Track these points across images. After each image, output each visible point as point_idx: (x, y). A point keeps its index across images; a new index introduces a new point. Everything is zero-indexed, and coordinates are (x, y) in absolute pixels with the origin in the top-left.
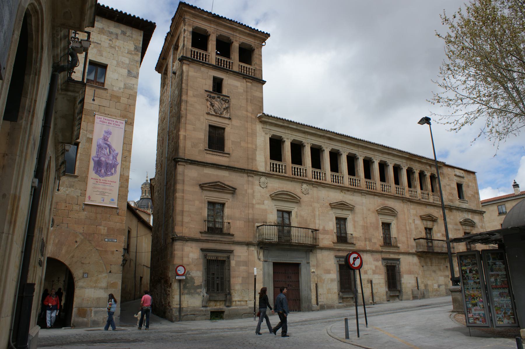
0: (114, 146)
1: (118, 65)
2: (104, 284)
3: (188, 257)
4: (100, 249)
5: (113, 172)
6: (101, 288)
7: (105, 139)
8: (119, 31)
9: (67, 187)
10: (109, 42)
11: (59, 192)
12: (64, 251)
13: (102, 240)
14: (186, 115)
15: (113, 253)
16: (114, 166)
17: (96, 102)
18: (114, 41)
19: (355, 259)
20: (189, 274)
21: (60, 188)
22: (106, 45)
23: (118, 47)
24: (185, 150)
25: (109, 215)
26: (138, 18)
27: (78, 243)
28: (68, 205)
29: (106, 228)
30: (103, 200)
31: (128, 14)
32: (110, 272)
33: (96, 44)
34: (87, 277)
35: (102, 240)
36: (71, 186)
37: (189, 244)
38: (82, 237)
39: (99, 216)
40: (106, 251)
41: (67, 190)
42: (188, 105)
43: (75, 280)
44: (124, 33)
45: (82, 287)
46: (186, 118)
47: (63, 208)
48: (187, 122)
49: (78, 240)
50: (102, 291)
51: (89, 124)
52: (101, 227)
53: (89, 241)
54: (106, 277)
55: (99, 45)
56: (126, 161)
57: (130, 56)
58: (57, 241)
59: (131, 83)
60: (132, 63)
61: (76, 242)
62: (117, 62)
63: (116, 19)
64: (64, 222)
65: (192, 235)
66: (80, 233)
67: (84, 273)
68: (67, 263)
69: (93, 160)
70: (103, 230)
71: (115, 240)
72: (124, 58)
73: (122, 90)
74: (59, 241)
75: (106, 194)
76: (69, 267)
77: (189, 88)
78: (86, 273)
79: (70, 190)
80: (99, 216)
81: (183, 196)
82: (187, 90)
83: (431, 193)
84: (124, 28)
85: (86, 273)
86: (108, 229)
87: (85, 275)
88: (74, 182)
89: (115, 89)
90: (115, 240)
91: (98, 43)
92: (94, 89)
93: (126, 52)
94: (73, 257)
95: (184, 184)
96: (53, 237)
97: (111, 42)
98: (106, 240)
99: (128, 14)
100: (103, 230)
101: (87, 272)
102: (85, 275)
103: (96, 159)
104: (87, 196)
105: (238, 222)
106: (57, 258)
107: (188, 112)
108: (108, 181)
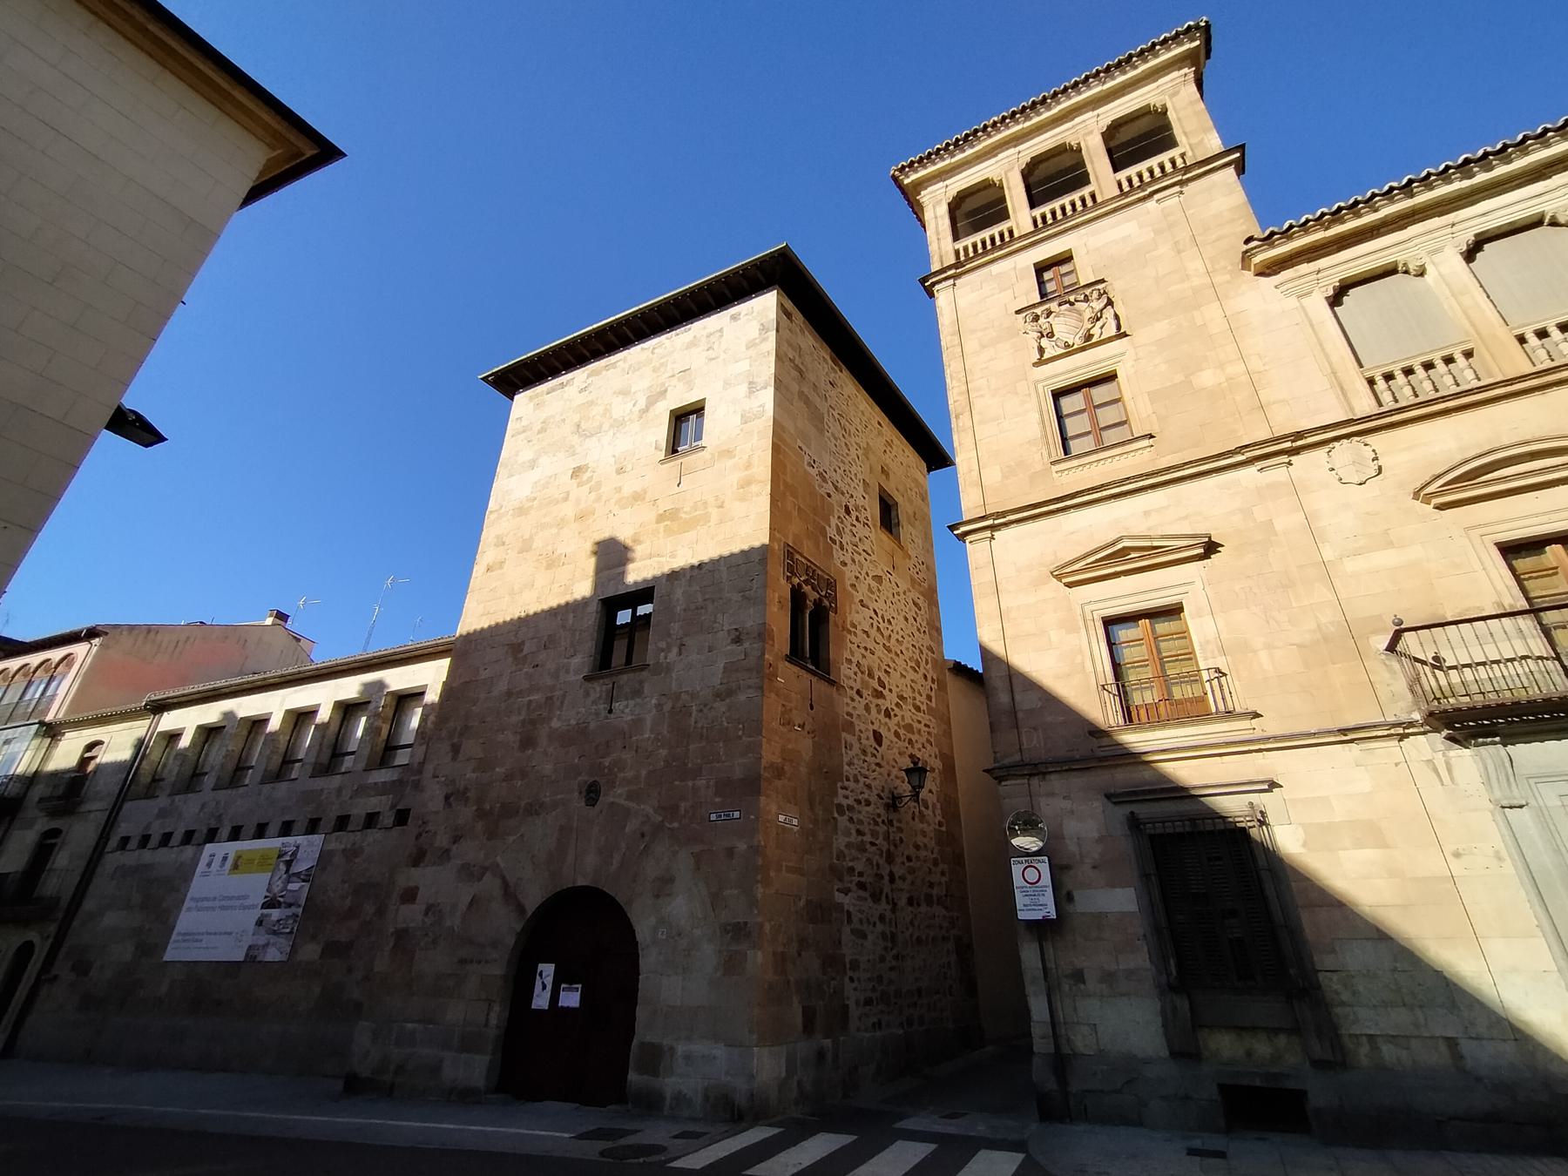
37: (1056, 782)
71: (737, 814)
90: (737, 814)
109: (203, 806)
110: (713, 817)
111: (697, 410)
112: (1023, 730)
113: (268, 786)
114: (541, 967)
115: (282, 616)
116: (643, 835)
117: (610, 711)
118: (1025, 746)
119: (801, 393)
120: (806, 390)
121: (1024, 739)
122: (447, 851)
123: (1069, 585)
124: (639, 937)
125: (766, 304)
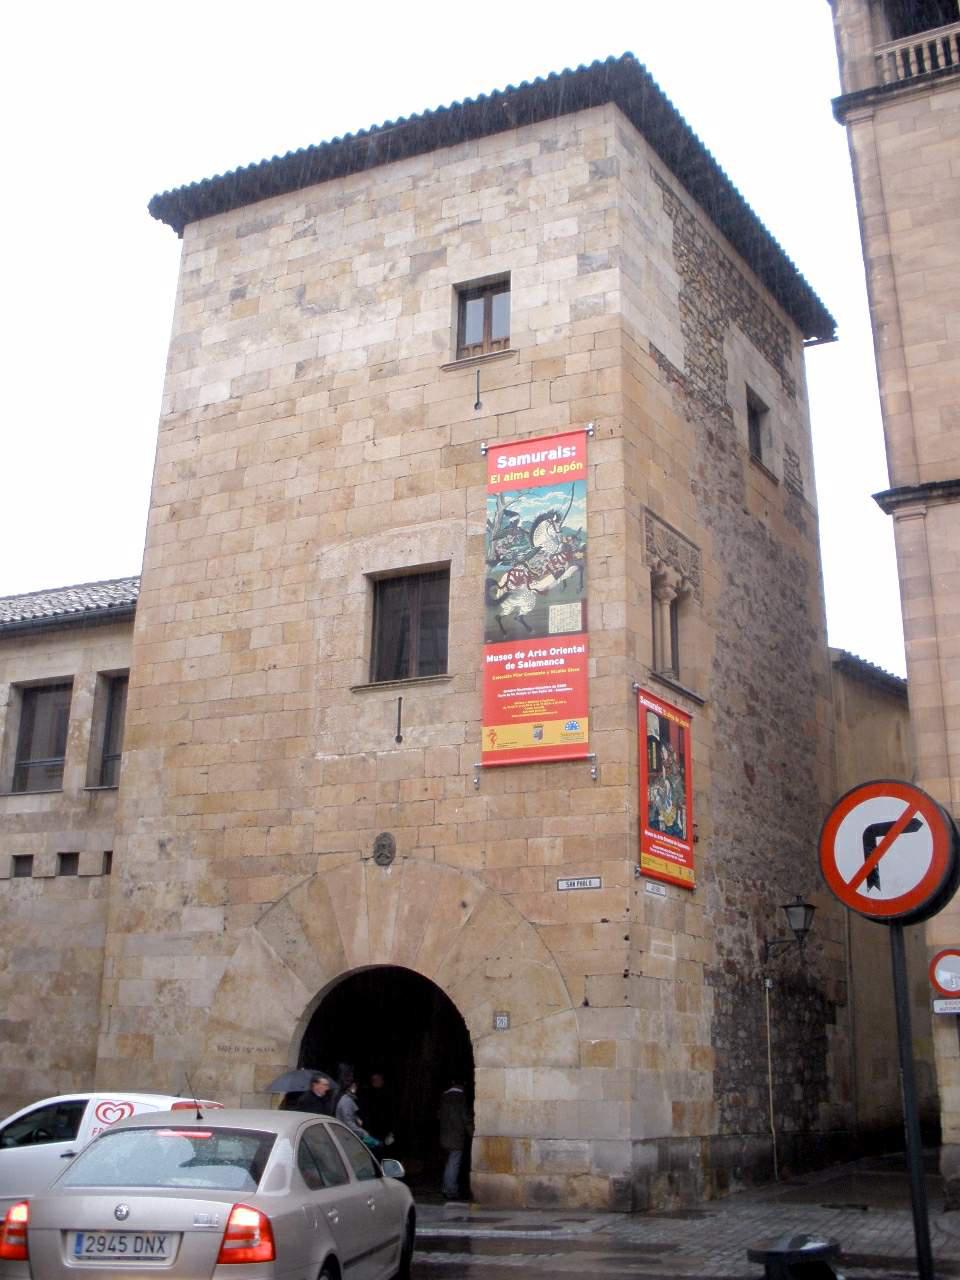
1: (544, 254)
2: (565, 1050)
4: (544, 921)
6: (557, 1065)
8: (533, 149)
9: (422, 723)
10: (505, 199)
12: (428, 941)
13: (548, 888)
14: (898, 310)
15: (589, 930)
17: (486, 410)
18: (519, 189)
19: (876, 838)
21: (406, 731)
22: (499, 212)
23: (536, 199)
24: (915, 452)
25: (563, 793)
26: (252, 166)
27: (470, 910)
28: (429, 782)
29: (559, 841)
32: (586, 1004)
33: (465, 229)
34: (508, 1027)
35: (548, 888)
36: (435, 716)
38: (482, 887)
39: (531, 802)
40: (564, 927)
41: (423, 733)
42: (899, 268)
43: (472, 1037)
44: (549, 147)
45: (495, 1065)
46: (899, 322)
47: (416, 797)
48: (908, 334)
49: (468, 897)
50: (561, 1077)
51: (471, 490)
52: (543, 841)
53: (506, 897)
54: (571, 1023)
55: (477, 227)
56: (608, 575)
57: (578, 206)
58: (406, 908)
59: (594, 292)
60: (590, 226)
61: (464, 905)
62: (539, 249)
63: (513, 118)
64: (423, 844)
66: (475, 874)
67: (495, 1014)
68: (440, 982)
70: (548, 849)
71: (596, 882)
72: (559, 224)
73: (566, 332)
74: (411, 910)
77: (890, 204)
78: (501, 1013)
79: (431, 730)
80: (531, 802)
81: (937, 646)
82: (884, 213)
84: (547, 130)
85: (501, 1013)
86: (566, 844)
87: (502, 1021)
88: (442, 701)
89: (541, 338)
90: (596, 882)
91: (471, 223)
92: (474, 370)
93: (566, 198)
94: (457, 959)
95: (931, 593)
96: (395, 897)
97: (512, 198)
98: (563, 885)
100: (548, 849)
101: (506, 1008)
102: (502, 1021)
106: (409, 966)
107: (902, 296)
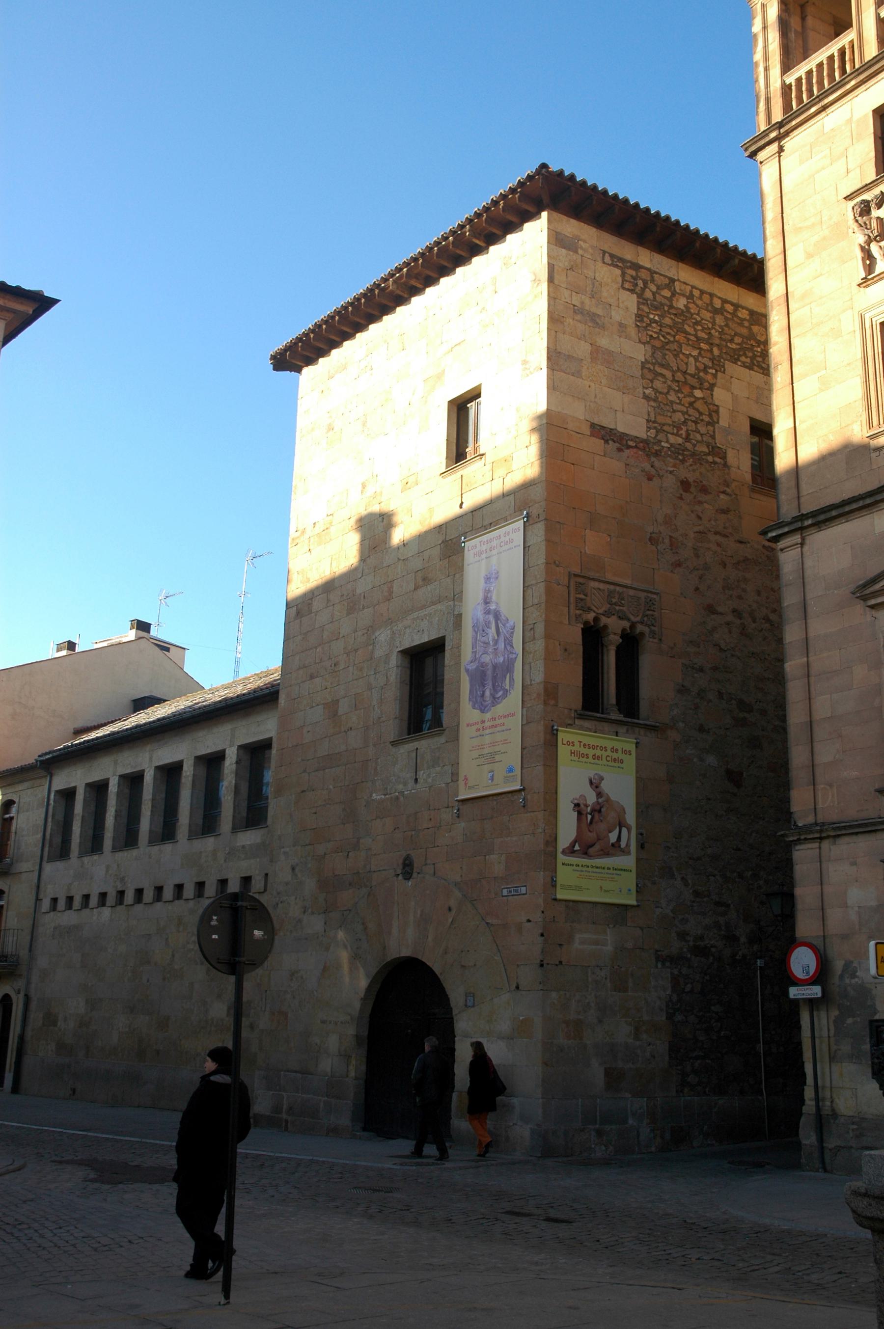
0: (504, 611)
3: (845, 906)
5: (507, 687)
7: (487, 601)
11: (418, 786)
16: (508, 667)
20: (853, 975)
27: (453, 912)
29: (503, 857)
30: (492, 779)
31: (566, 174)
32: (517, 988)
34: (473, 1006)
37: (845, 847)
65: (852, 813)
66: (456, 884)
67: (467, 995)
68: (437, 969)
69: (467, 671)
71: (523, 890)
75: (497, 758)
76: (441, 978)
83: (576, 300)
90: (523, 890)
99: (566, 174)
103: (473, 666)
104: (461, 778)
105: (374, 796)
108: (500, 717)
109: (108, 867)
110: (505, 892)
111: (474, 395)
112: (820, 787)
113: (156, 848)
114: (791, 996)
115: (143, 626)
116: (450, 909)
117: (416, 780)
118: (820, 805)
119: (597, 352)
120: (604, 342)
121: (820, 795)
122: (300, 921)
123: (872, 607)
124: (453, 1004)
125: (533, 238)
